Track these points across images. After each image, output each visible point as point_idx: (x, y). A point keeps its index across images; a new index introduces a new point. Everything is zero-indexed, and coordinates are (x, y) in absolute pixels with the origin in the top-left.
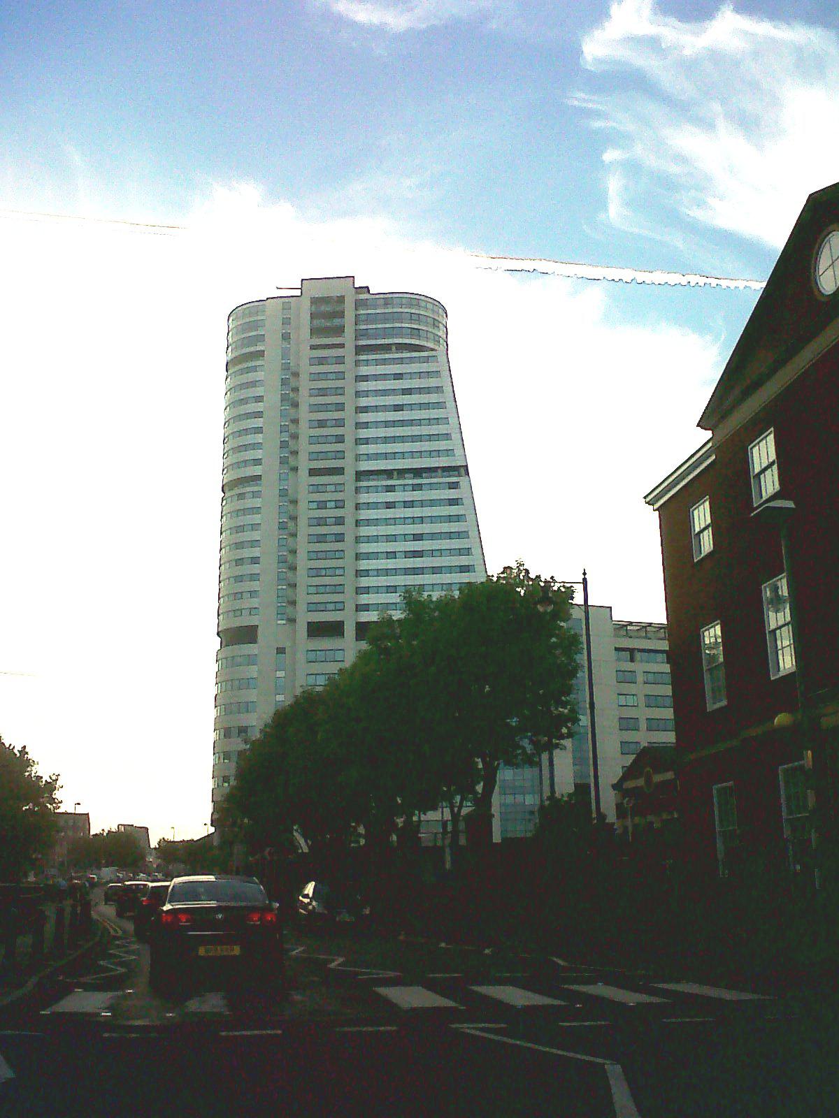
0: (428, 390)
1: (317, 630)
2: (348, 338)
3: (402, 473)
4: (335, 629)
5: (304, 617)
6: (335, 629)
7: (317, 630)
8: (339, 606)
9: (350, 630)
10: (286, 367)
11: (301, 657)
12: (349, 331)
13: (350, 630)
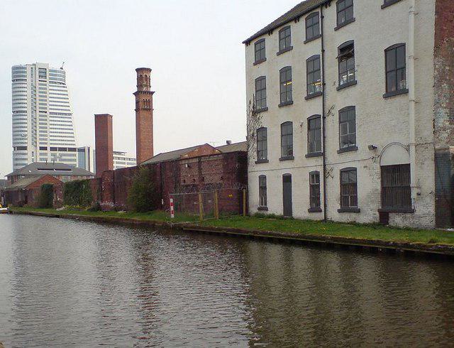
1: (41, 148)
2: (48, 80)
3: (56, 113)
4: (46, 149)
5: (39, 146)
6: (46, 149)
7: (41, 148)
8: (46, 144)
9: (49, 149)
11: (38, 154)
13: (49, 149)
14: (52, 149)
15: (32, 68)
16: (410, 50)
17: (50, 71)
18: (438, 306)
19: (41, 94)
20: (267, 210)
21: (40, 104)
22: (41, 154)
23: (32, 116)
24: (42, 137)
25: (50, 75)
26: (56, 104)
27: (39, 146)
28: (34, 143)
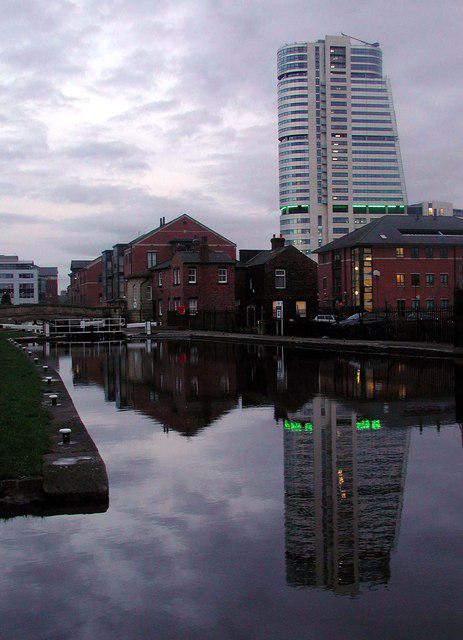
0: (395, 184)
1: (336, 209)
2: (348, 70)
4: (345, 209)
5: (331, 203)
6: (345, 209)
7: (336, 209)
8: (346, 198)
9: (351, 210)
10: (318, 82)
11: (330, 220)
12: (349, 63)
14: (357, 211)
15: (317, 48)
16: (81, 530)
17: (354, 51)
18: (99, 565)
19: (336, 123)
20: (53, 271)
21: (334, 182)
22: (336, 220)
23: (318, 144)
24: (339, 179)
25: (353, 59)
26: (377, 164)
27: (331, 203)
28: (322, 199)
